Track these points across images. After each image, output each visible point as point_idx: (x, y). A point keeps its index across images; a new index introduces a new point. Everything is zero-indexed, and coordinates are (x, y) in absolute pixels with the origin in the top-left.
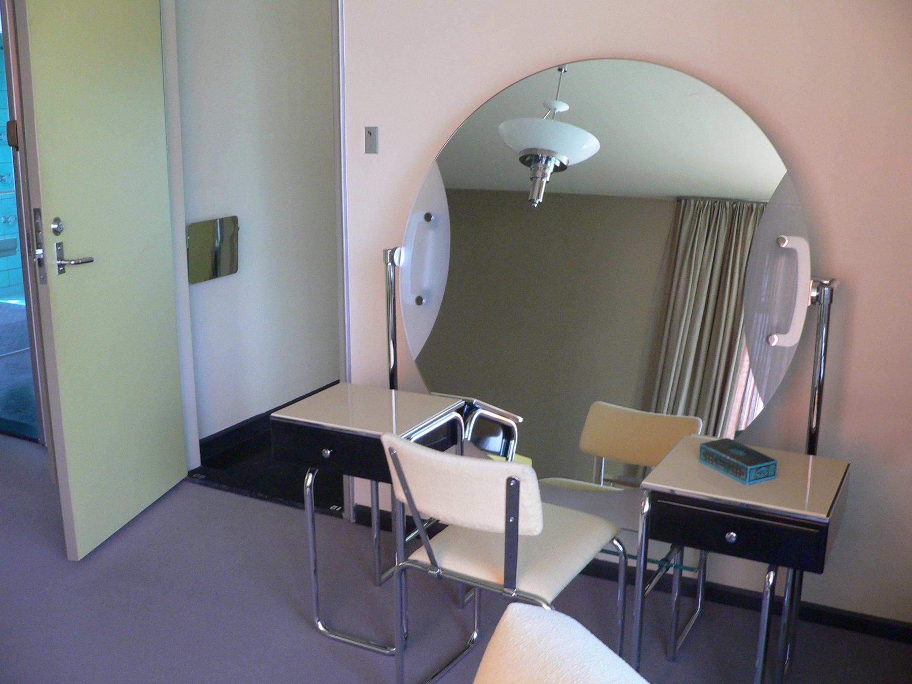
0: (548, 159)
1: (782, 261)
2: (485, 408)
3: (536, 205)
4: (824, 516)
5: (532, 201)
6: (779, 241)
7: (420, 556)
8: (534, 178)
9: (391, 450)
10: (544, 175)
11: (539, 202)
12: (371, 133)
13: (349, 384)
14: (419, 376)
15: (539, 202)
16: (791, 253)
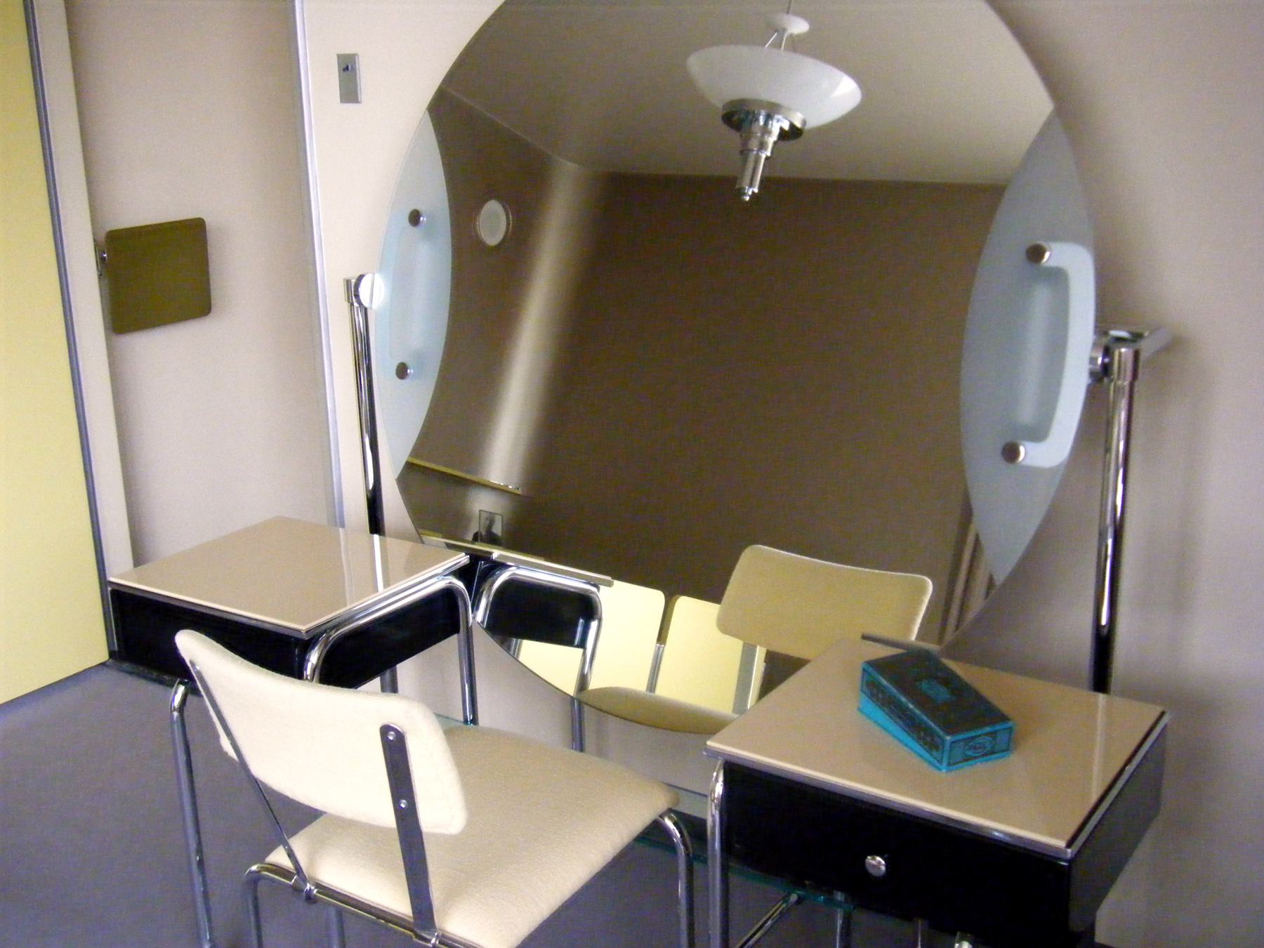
0: (769, 117)
1: (1041, 296)
2: (519, 564)
3: (747, 198)
4: (1061, 843)
5: (741, 192)
6: (1036, 253)
7: (279, 857)
8: (744, 152)
9: (191, 662)
10: (762, 146)
11: (753, 192)
12: (348, 67)
13: (341, 530)
14: (404, 505)
15: (753, 192)
16: (1058, 277)
